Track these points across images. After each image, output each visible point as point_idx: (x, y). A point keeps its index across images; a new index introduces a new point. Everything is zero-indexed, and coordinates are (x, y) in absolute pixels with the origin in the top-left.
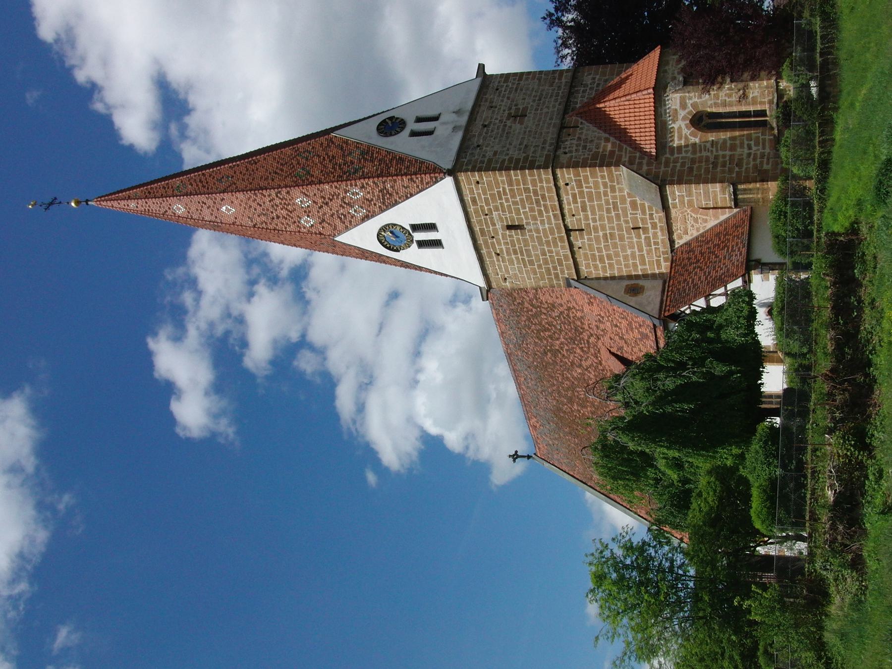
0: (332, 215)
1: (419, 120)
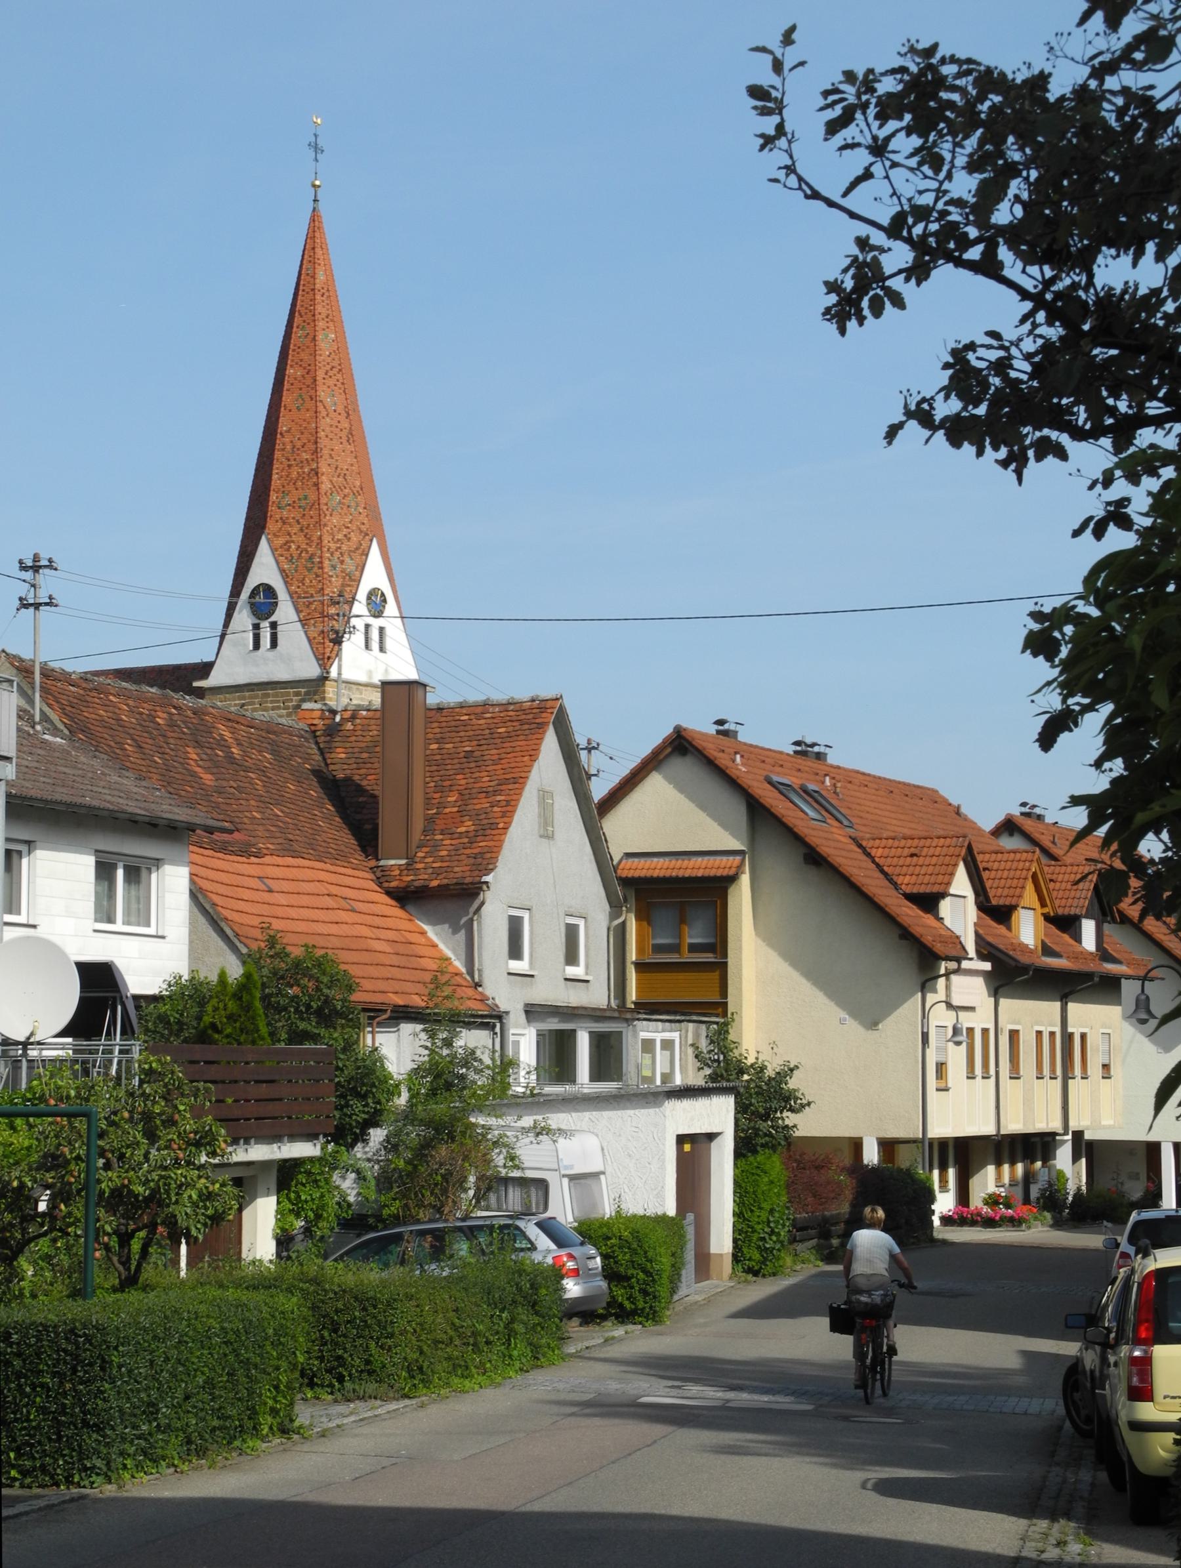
0: (289, 534)
1: (382, 630)
